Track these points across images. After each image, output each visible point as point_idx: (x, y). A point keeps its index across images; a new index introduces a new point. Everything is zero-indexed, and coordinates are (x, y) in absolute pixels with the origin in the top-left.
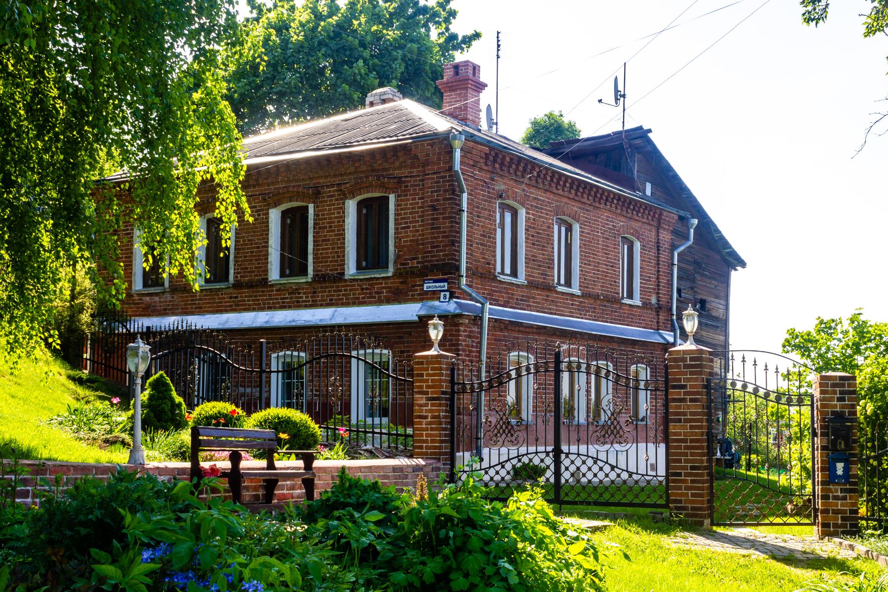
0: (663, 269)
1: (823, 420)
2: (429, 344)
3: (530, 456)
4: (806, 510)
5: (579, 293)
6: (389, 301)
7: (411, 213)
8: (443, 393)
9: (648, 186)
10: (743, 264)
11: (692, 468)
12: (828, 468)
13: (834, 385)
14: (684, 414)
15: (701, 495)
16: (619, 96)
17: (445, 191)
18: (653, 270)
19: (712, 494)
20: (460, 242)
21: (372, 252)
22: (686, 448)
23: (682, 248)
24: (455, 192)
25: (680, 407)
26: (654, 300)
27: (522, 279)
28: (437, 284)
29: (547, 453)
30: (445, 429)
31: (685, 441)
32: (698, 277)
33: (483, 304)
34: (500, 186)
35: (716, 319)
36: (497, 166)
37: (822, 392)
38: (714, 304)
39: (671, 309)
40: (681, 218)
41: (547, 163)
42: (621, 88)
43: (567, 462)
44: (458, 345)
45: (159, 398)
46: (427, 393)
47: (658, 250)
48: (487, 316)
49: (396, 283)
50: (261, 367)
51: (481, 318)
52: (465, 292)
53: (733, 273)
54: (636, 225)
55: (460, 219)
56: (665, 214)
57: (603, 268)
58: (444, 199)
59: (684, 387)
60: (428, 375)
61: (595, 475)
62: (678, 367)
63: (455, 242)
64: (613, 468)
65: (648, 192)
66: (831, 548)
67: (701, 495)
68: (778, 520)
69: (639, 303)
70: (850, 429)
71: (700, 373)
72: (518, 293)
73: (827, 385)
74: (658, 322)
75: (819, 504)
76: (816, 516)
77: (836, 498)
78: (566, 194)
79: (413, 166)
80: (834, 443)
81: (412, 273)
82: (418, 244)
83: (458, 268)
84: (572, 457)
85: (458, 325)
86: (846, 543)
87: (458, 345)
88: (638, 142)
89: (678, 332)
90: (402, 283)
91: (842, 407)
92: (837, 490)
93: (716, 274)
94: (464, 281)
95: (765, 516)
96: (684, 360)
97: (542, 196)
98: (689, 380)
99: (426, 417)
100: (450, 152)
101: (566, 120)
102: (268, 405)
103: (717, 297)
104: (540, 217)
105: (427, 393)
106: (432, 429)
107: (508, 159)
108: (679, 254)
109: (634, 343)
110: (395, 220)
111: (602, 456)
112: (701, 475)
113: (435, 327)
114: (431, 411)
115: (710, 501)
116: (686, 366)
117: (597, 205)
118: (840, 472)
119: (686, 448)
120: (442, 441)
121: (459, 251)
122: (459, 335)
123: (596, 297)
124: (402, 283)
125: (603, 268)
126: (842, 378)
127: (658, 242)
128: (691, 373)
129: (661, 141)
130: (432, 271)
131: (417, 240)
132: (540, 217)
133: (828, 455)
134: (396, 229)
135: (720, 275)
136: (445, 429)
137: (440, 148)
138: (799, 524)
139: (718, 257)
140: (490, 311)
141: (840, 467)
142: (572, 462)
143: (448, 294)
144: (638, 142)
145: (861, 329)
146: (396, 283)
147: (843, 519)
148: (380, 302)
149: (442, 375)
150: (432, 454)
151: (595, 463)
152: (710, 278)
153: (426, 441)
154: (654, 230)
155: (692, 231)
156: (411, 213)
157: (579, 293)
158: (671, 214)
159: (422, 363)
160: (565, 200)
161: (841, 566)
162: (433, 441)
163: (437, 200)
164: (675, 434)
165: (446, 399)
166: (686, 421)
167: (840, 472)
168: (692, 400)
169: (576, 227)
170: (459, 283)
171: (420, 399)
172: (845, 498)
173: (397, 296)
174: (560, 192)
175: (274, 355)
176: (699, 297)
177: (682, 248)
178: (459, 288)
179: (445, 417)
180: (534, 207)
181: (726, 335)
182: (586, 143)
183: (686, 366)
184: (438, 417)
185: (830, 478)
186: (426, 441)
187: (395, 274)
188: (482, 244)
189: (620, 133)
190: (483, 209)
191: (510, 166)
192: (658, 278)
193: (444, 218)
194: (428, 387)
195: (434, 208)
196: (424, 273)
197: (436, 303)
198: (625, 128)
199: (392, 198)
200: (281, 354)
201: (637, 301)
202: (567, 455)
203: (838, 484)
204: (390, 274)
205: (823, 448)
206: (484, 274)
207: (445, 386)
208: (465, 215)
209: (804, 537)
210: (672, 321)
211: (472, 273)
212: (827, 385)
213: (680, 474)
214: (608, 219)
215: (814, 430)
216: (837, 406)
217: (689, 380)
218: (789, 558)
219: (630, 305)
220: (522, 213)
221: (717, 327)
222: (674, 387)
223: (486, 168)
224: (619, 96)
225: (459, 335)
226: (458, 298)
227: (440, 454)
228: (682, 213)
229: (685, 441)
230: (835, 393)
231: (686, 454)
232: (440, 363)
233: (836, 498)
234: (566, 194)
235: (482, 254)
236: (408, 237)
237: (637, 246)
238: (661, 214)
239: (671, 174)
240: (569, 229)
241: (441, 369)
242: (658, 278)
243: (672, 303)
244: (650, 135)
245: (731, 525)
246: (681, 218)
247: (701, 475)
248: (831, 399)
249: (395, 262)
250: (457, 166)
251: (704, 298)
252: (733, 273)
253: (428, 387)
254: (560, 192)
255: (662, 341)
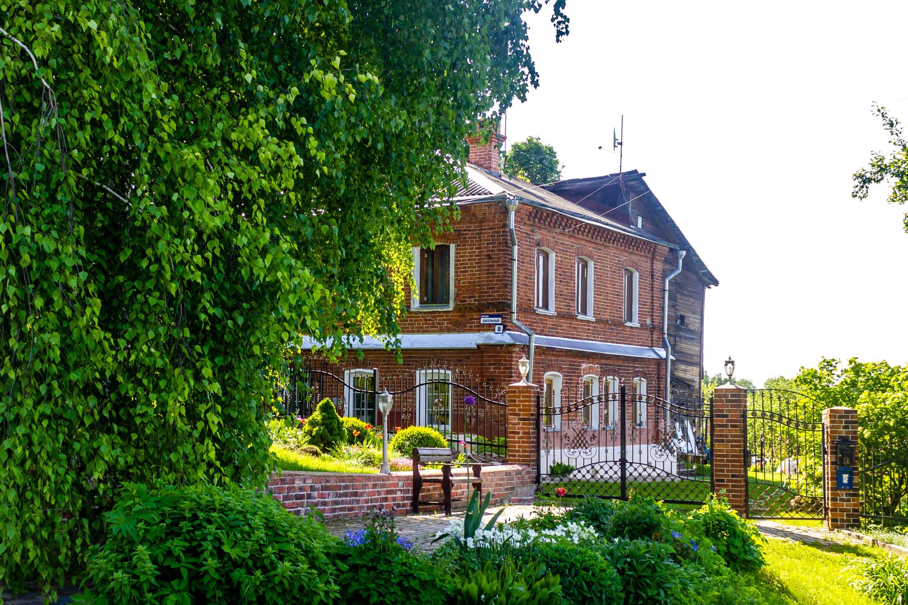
0: (657, 294)
1: (832, 442)
2: (520, 377)
3: (601, 464)
4: (814, 507)
5: (593, 320)
6: (449, 331)
7: (469, 260)
8: (532, 415)
9: (640, 219)
10: (716, 283)
11: (732, 476)
12: (837, 478)
13: (840, 417)
14: (727, 436)
15: (740, 497)
16: (618, 143)
17: (500, 244)
18: (649, 296)
19: (747, 495)
20: (511, 285)
21: (433, 289)
22: (728, 461)
23: (672, 276)
24: (506, 245)
25: (723, 431)
26: (649, 322)
27: (552, 311)
28: (493, 319)
29: (615, 463)
30: (532, 442)
31: (727, 456)
32: (679, 296)
33: (530, 335)
34: (538, 236)
35: (693, 332)
36: (537, 220)
37: (831, 422)
38: (691, 319)
39: (662, 329)
40: (671, 250)
41: (568, 212)
42: (618, 137)
43: (631, 469)
44: (511, 368)
45: (329, 418)
46: (519, 415)
47: (652, 278)
48: (533, 345)
49: (456, 317)
50: (374, 390)
51: (529, 347)
52: (517, 326)
53: (707, 290)
54: (635, 258)
55: (512, 266)
56: (659, 247)
57: (610, 297)
58: (499, 250)
59: (726, 416)
60: (519, 401)
61: (606, 472)
62: (722, 401)
63: (507, 285)
64: (668, 474)
65: (640, 226)
66: (841, 537)
67: (740, 497)
68: (787, 516)
69: (638, 325)
70: (853, 449)
71: (739, 406)
72: (550, 322)
73: (835, 416)
74: (652, 340)
75: (830, 505)
76: (826, 514)
77: (842, 500)
78: (585, 237)
79: (470, 222)
80: (841, 460)
81: (471, 308)
82: (475, 286)
83: (510, 306)
84: (635, 466)
85: (511, 352)
86: (854, 534)
87: (511, 368)
88: (633, 183)
89: (670, 348)
90: (461, 316)
91: (847, 433)
92: (843, 494)
93: (693, 292)
94: (515, 316)
95: (777, 512)
96: (726, 396)
97: (567, 241)
98: (730, 411)
99: (518, 433)
100: (506, 212)
101: (544, 142)
102: (412, 422)
103: (694, 313)
104: (566, 258)
105: (519, 415)
106: (523, 442)
107: (545, 214)
108: (670, 282)
109: (635, 359)
110: (456, 265)
111: (660, 466)
112: (740, 482)
113: (524, 364)
114: (522, 428)
115: (746, 501)
116: (727, 401)
117: (607, 244)
118: (845, 481)
119: (728, 461)
120: (531, 452)
121: (511, 292)
122: (512, 361)
123: (605, 322)
124: (461, 316)
125: (610, 297)
126: (846, 411)
127: (652, 272)
128: (732, 406)
129: (659, 186)
130: (488, 308)
131: (475, 282)
132: (566, 258)
133: (836, 469)
134: (456, 272)
135: (696, 293)
136: (532, 442)
137: (496, 209)
138: (813, 519)
139: (694, 277)
140: (537, 340)
141: (845, 478)
142: (635, 469)
143: (502, 327)
144: (633, 183)
145: (857, 369)
146: (456, 317)
147: (848, 516)
148: (441, 331)
149: (530, 401)
150: (523, 461)
151: (654, 470)
152: (688, 296)
153: (518, 451)
154: (649, 261)
155: (681, 261)
156: (469, 260)
157: (593, 320)
158: (663, 247)
159: (515, 392)
160: (584, 243)
161: (854, 550)
162: (524, 451)
163: (492, 251)
164: (719, 451)
165: (533, 420)
166: (728, 441)
167: (845, 481)
168: (732, 426)
169: (591, 264)
170: (511, 318)
171: (513, 419)
172: (849, 500)
173: (458, 326)
174: (580, 236)
175: (347, 372)
176: (679, 313)
177: (672, 276)
178: (511, 322)
179: (533, 433)
180: (562, 252)
181: (701, 347)
182: (586, 183)
183: (727, 401)
184: (528, 433)
185: (838, 485)
186: (518, 451)
187: (455, 309)
188: (525, 285)
189: (618, 175)
190: (526, 256)
191: (546, 219)
192: (652, 303)
193: (498, 266)
194: (519, 410)
195: (489, 257)
196: (481, 309)
197: (492, 334)
198: (624, 170)
199: (453, 247)
200: (352, 371)
201: (635, 323)
202: (631, 464)
203: (844, 490)
204: (451, 309)
205: (832, 463)
206: (527, 309)
207: (533, 410)
208: (516, 264)
209: (819, 529)
210: (663, 339)
211: (520, 308)
212: (835, 416)
213: (723, 481)
214: (615, 255)
215: (824, 449)
216: (843, 432)
217: (730, 411)
218: (807, 541)
219: (631, 327)
220: (553, 257)
221: (694, 339)
222: (718, 416)
223: (528, 222)
224: (618, 143)
225: (512, 361)
226: (509, 330)
227: (530, 461)
228: (672, 246)
229: (727, 456)
230: (841, 422)
231: (728, 466)
232: (529, 392)
233: (842, 500)
234: (585, 237)
235: (525, 292)
236: (467, 279)
237: (636, 276)
238: (656, 248)
239: (659, 208)
240: (585, 266)
241: (530, 397)
242: (652, 303)
243: (663, 323)
244: (643, 178)
245: (762, 519)
246: (671, 250)
247: (740, 482)
248: (838, 427)
249: (455, 300)
250: (512, 225)
251: (683, 314)
252: (707, 290)
253: (519, 410)
254: (580, 236)
255: (655, 357)
